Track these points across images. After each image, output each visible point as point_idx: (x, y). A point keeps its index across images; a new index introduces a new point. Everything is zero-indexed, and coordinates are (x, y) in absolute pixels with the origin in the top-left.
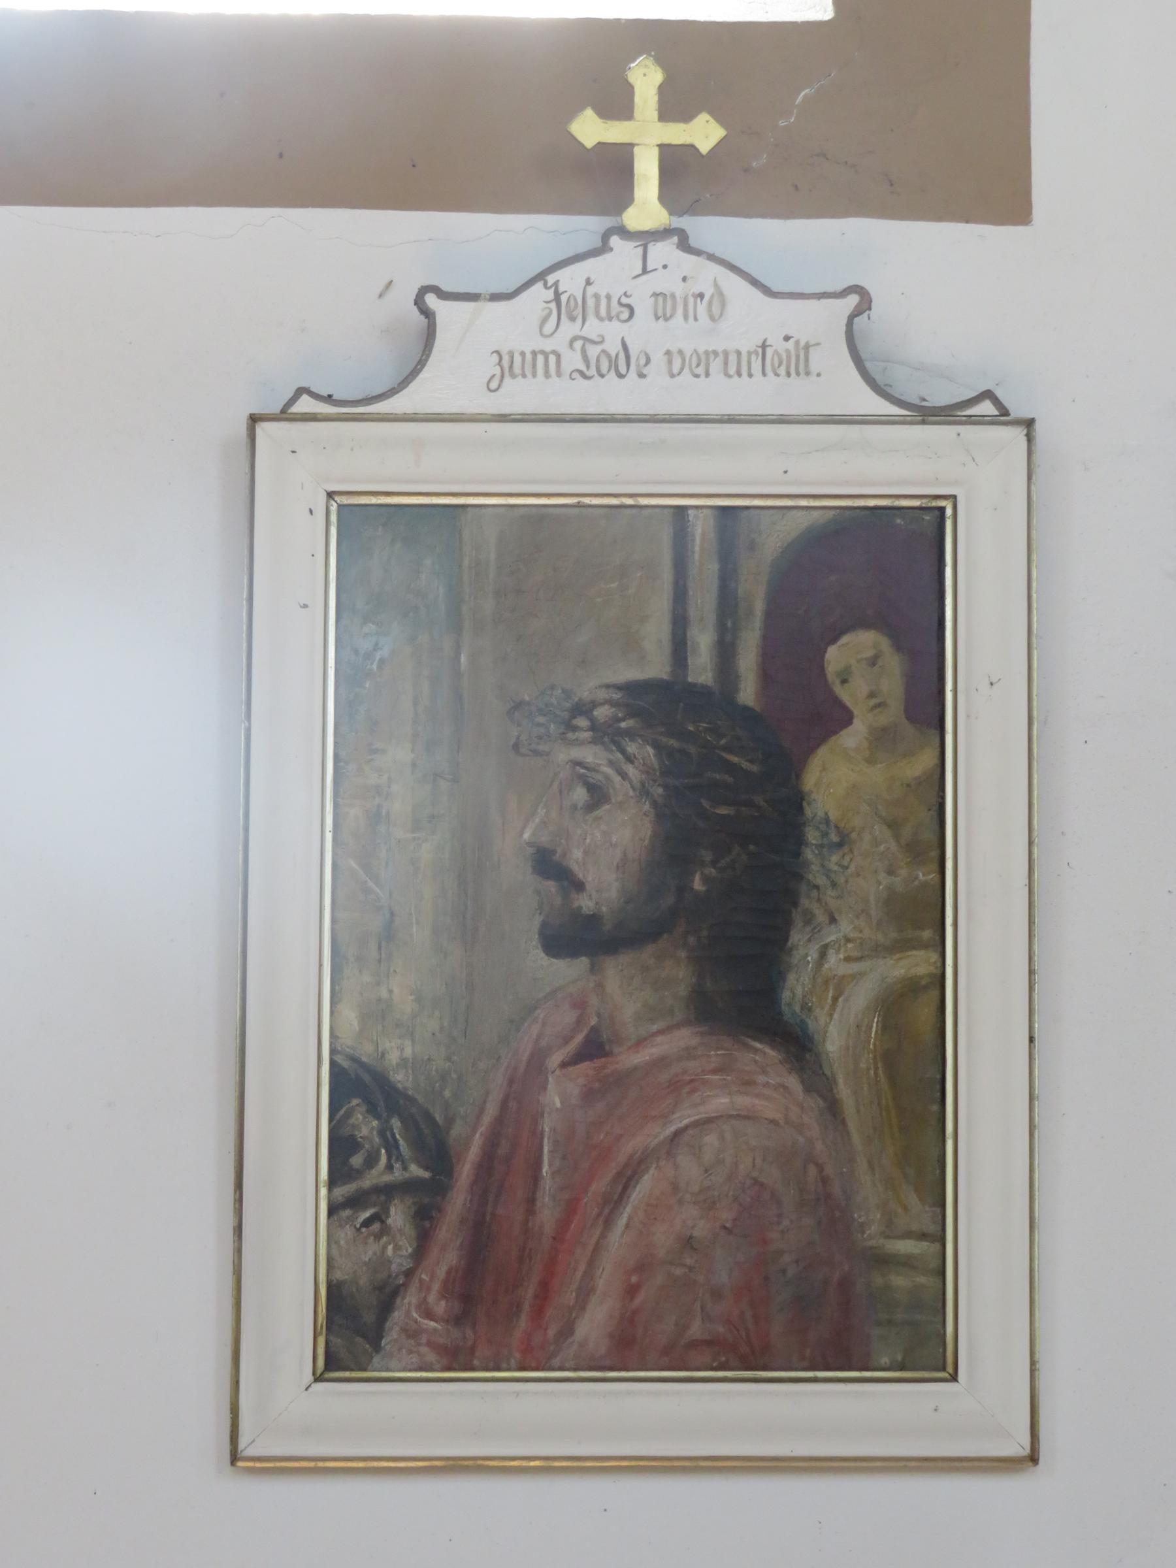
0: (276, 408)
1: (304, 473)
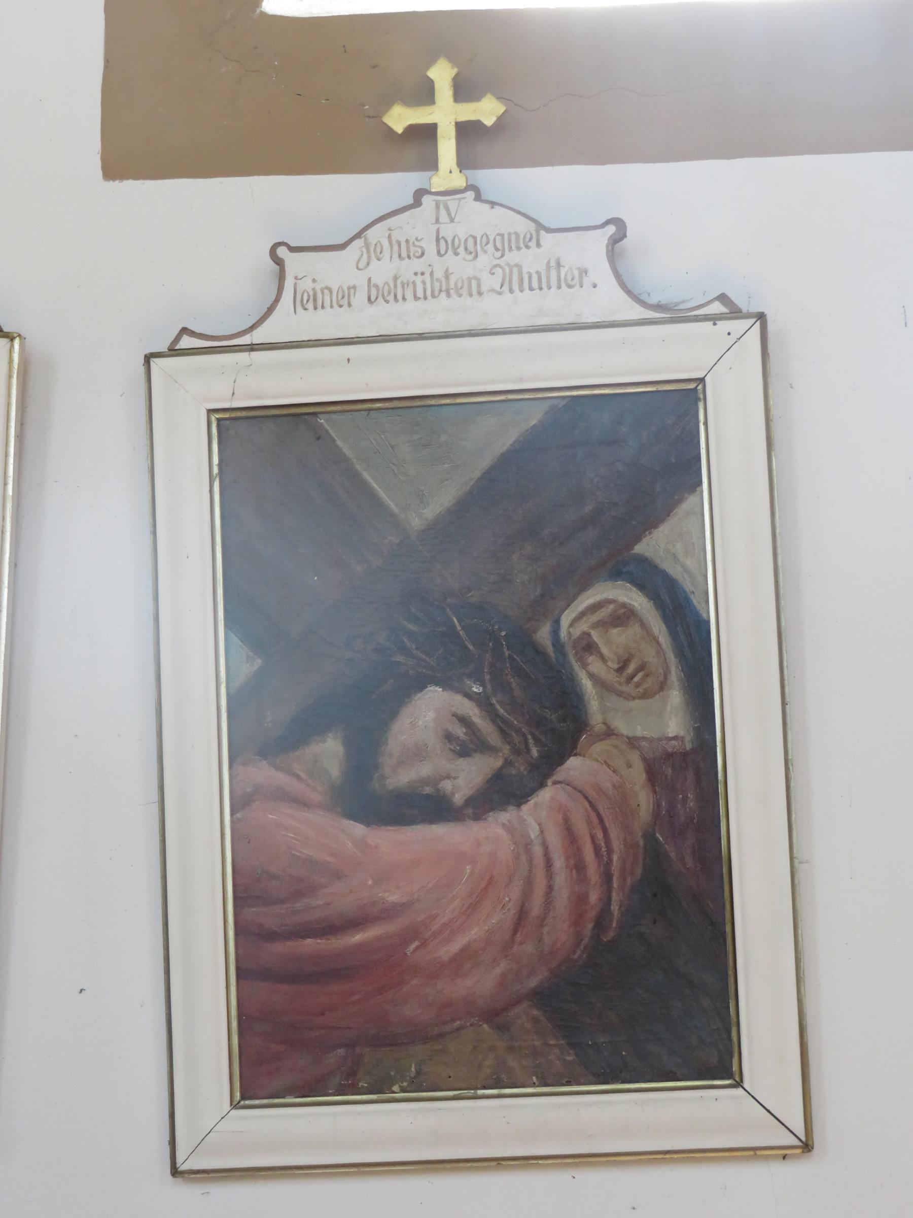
0: (164, 348)
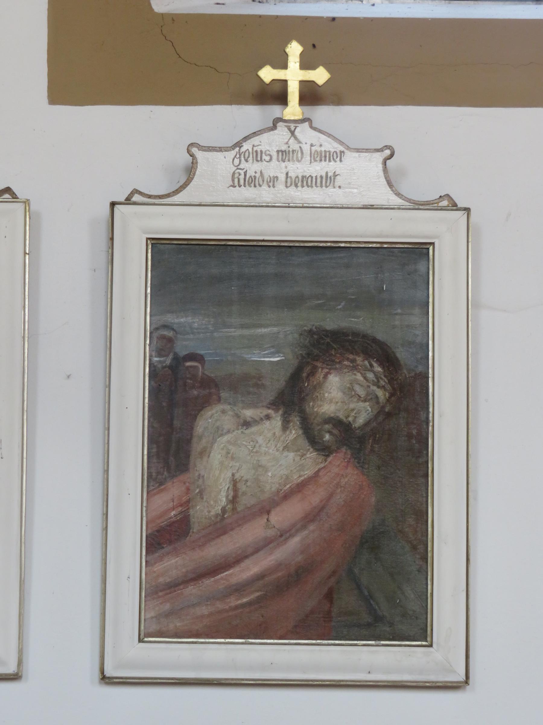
0: (122, 199)
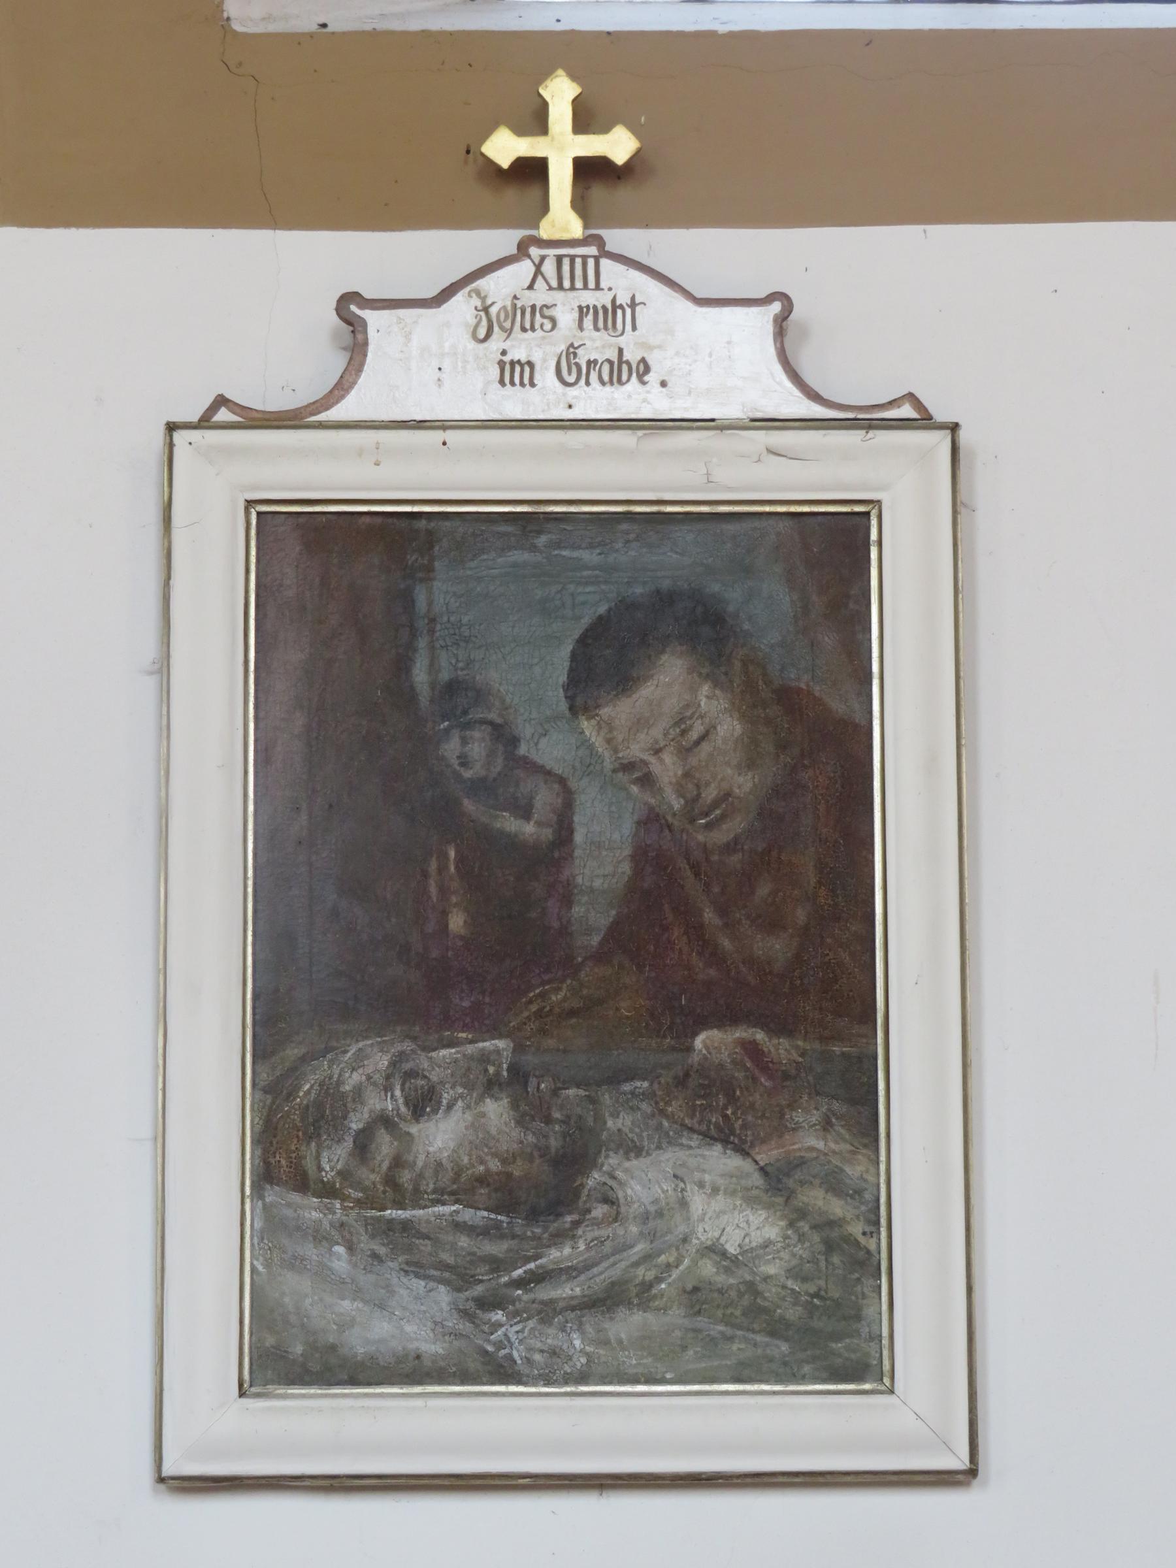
0: (195, 418)
1: (223, 486)
